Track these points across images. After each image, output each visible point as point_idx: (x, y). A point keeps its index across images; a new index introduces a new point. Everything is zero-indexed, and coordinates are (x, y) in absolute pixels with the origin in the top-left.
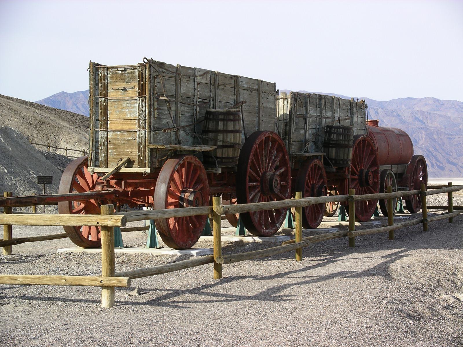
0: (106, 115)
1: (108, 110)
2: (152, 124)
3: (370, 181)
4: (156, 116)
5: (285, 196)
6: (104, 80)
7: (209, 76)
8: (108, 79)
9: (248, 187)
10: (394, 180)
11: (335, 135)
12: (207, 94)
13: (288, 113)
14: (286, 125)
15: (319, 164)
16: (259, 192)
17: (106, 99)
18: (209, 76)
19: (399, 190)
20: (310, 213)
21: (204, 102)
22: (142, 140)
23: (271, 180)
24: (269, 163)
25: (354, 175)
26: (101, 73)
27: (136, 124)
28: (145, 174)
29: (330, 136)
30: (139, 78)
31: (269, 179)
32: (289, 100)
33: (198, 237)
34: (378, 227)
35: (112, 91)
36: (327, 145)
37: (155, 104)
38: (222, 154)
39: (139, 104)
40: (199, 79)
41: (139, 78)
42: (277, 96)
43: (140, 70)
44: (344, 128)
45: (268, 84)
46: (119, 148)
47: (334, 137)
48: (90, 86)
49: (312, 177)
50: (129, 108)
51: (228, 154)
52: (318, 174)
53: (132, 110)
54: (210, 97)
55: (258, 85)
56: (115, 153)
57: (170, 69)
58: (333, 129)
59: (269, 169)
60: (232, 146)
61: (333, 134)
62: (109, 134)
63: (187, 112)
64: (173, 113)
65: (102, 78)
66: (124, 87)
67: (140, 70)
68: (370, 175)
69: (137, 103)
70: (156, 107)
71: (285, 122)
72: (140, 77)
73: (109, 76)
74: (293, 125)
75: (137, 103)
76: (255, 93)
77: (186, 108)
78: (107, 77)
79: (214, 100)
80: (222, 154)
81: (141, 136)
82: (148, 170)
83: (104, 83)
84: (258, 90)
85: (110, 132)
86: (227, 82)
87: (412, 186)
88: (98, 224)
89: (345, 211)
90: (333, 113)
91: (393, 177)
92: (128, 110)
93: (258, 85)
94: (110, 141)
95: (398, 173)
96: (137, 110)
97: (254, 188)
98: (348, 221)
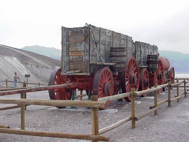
2: (91, 53)
4: (92, 49)
7: (111, 32)
8: (70, 34)
9: (126, 80)
10: (166, 77)
12: (110, 41)
18: (111, 32)
21: (109, 43)
28: (87, 76)
29: (149, 59)
30: (84, 33)
36: (148, 63)
37: (92, 44)
38: (119, 66)
39: (84, 44)
40: (107, 34)
41: (84, 33)
43: (85, 29)
44: (155, 56)
45: (130, 37)
46: (75, 64)
47: (151, 59)
50: (79, 46)
51: (121, 66)
53: (81, 47)
54: (111, 42)
55: (127, 37)
57: (97, 29)
60: (124, 63)
63: (103, 48)
64: (98, 49)
65: (67, 33)
67: (85, 29)
69: (83, 44)
70: (92, 46)
72: (85, 32)
75: (83, 44)
76: (126, 41)
77: (103, 46)
79: (113, 43)
80: (119, 66)
81: (85, 58)
82: (89, 74)
84: (127, 40)
86: (116, 36)
87: (156, 77)
88: (91, 107)
90: (149, 50)
92: (79, 47)
93: (127, 37)
96: (83, 47)
97: (127, 80)
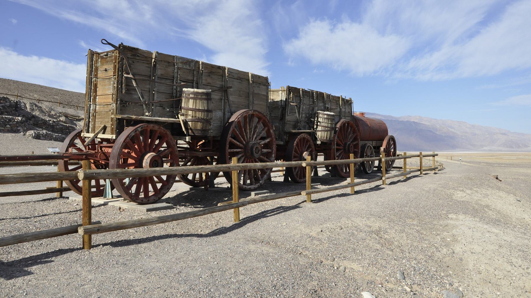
0: (96, 91)
1: (97, 87)
3: (351, 150)
5: (270, 160)
6: (96, 64)
10: (372, 150)
11: (321, 119)
13: (285, 100)
14: (283, 110)
15: (307, 137)
16: (242, 156)
17: (96, 79)
19: (376, 156)
20: (299, 172)
22: (113, 111)
23: (252, 148)
24: (254, 134)
25: (340, 146)
26: (95, 59)
27: (202, 108)
31: (250, 147)
32: (285, 92)
33: (169, 188)
34: (122, 187)
35: (101, 72)
42: (269, 86)
48: (87, 69)
49: (301, 146)
52: (306, 145)
56: (99, 122)
58: (320, 115)
59: (254, 139)
61: (320, 118)
62: (97, 106)
65: (95, 61)
66: (106, 69)
68: (351, 147)
71: (282, 108)
73: (99, 60)
74: (288, 109)
78: (98, 61)
83: (96, 66)
85: (98, 105)
89: (314, 170)
91: (372, 148)
94: (97, 112)
95: (377, 146)
98: (105, 181)
